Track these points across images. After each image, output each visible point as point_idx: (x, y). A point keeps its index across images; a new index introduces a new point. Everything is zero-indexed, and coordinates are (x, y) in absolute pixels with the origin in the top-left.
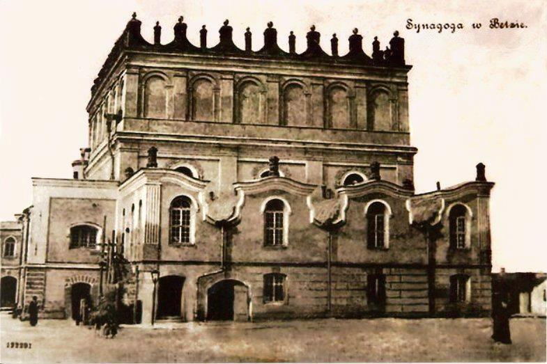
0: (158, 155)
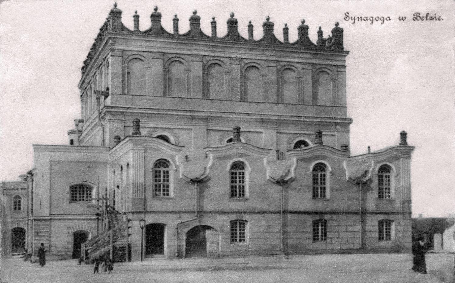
0: (141, 125)
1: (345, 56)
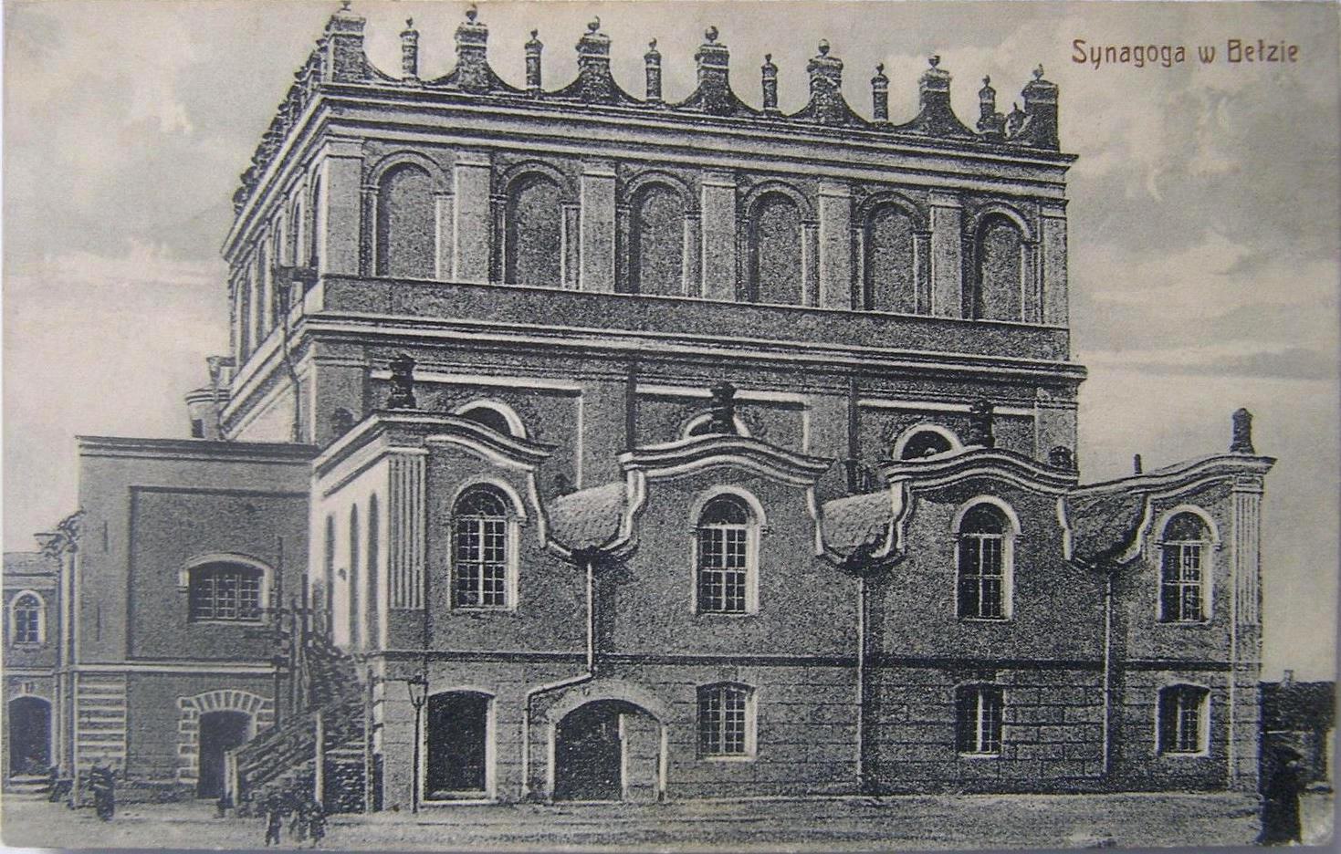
1: (1066, 169)
